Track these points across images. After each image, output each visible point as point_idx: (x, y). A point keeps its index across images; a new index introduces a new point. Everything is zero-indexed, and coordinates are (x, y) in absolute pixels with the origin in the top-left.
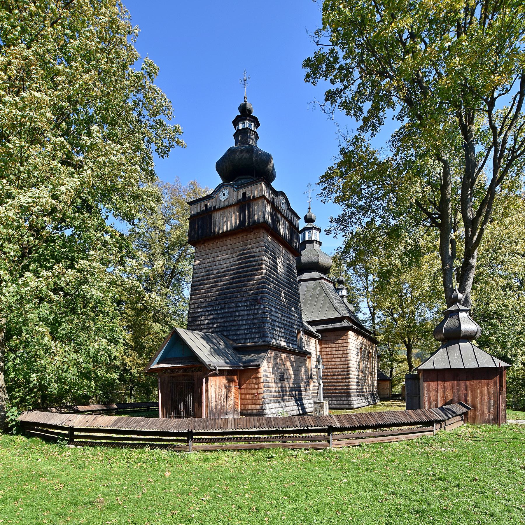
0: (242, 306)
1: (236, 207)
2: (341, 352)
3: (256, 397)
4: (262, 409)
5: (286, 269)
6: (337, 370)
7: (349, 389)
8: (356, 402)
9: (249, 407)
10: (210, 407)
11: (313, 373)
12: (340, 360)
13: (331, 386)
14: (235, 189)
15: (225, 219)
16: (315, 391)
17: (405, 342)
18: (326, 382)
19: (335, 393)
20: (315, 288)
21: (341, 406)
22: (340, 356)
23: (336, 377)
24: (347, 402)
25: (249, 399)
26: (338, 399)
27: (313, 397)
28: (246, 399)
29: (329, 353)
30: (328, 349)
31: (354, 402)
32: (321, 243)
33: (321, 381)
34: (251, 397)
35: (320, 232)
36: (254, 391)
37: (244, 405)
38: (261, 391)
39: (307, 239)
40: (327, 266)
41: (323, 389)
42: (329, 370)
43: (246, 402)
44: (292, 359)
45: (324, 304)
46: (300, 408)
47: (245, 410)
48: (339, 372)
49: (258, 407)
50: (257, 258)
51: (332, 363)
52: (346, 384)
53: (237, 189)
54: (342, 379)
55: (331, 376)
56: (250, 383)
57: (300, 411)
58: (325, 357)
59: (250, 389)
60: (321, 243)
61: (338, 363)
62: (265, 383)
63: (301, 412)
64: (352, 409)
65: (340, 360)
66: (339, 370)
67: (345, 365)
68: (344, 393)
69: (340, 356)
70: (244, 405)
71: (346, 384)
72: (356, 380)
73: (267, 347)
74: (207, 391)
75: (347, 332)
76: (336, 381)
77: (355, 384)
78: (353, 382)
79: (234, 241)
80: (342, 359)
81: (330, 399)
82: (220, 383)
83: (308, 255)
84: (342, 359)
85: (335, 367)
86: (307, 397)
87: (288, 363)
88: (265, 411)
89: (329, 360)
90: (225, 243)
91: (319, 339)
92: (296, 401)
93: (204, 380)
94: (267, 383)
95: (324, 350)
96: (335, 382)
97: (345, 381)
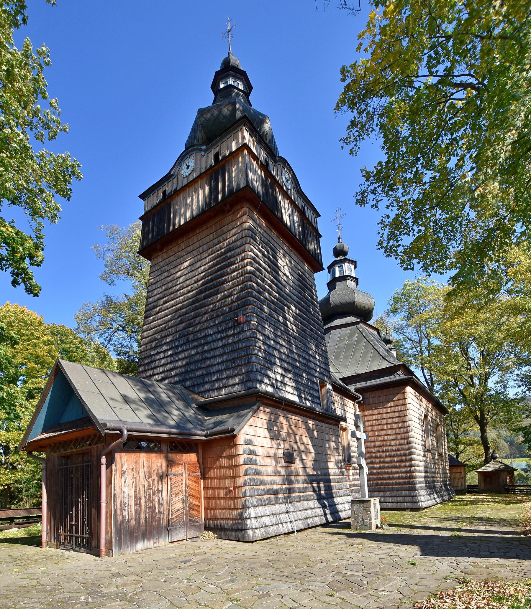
0: (214, 333)
1: (204, 180)
2: (396, 420)
3: (231, 494)
4: (242, 518)
5: (297, 282)
6: (391, 448)
7: (413, 477)
8: (425, 499)
9: (220, 514)
10: (119, 518)
11: (352, 454)
12: (394, 432)
13: (382, 473)
14: (203, 153)
15: (189, 201)
16: (357, 483)
17: (476, 418)
18: (374, 468)
19: (390, 484)
20: (351, 336)
21: (399, 505)
22: (394, 426)
23: (389, 459)
24: (410, 499)
25: (219, 498)
26: (394, 493)
27: (352, 492)
28: (214, 498)
29: (377, 423)
30: (374, 417)
31: (422, 498)
32: (357, 279)
33: (363, 462)
34: (222, 493)
35: (355, 267)
36: (228, 483)
37: (212, 509)
38: (240, 481)
39: (337, 275)
40: (367, 307)
41: (369, 480)
42: (378, 449)
43: (214, 503)
44: (311, 426)
45: (366, 353)
46: (328, 512)
47: (213, 519)
48: (393, 451)
49: (234, 514)
50: (237, 251)
51: (382, 438)
52: (407, 469)
53: (205, 151)
54: (399, 461)
55: (380, 457)
56: (220, 468)
57: (329, 516)
58: (370, 429)
59: (220, 478)
60: (357, 279)
61: (392, 437)
62: (247, 466)
63: (330, 519)
64: (419, 509)
65: (394, 432)
66: (394, 448)
67: (404, 439)
68: (405, 483)
69: (394, 426)
70: (212, 509)
71: (407, 469)
72: (422, 464)
73: (251, 400)
74: (109, 482)
75: (404, 388)
76: (390, 465)
77: (422, 469)
78: (418, 466)
79: (204, 234)
80: (399, 431)
81: (381, 494)
82: (149, 467)
83: (340, 294)
84: (399, 431)
85: (388, 443)
86: (342, 492)
87: (301, 432)
88: (248, 522)
89: (377, 433)
90: (191, 241)
91: (359, 403)
92: (320, 498)
93: (104, 460)
94: (254, 467)
95: (368, 418)
96: (388, 468)
97: (404, 464)
